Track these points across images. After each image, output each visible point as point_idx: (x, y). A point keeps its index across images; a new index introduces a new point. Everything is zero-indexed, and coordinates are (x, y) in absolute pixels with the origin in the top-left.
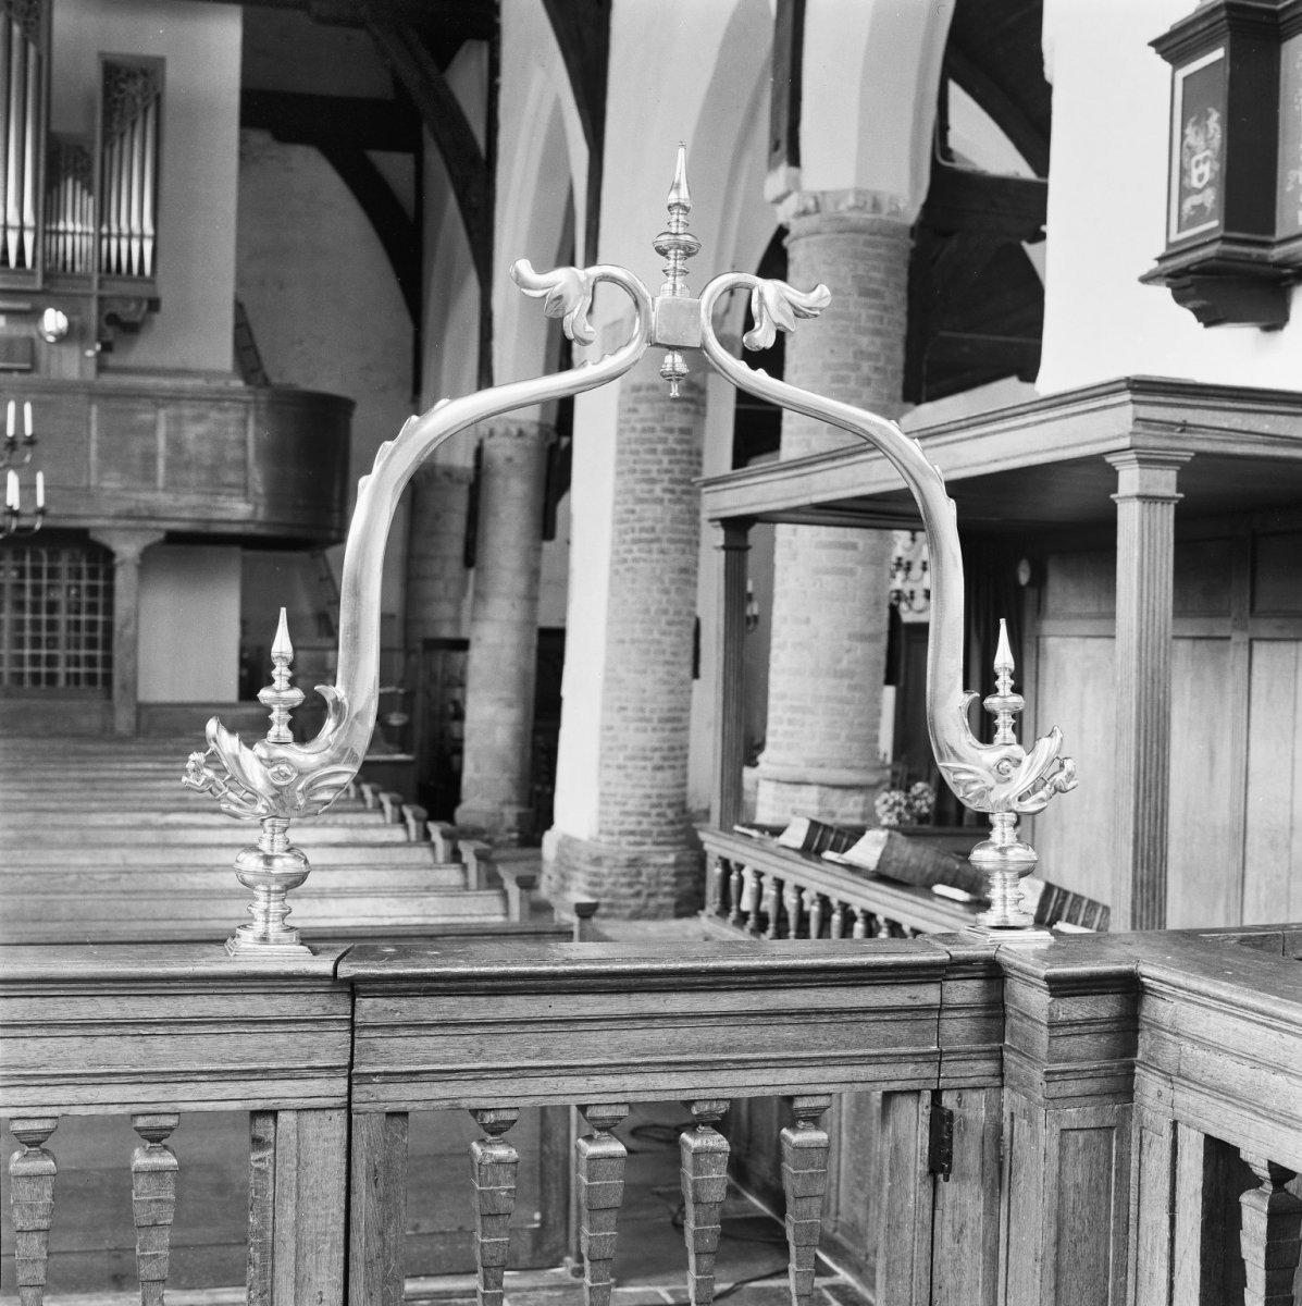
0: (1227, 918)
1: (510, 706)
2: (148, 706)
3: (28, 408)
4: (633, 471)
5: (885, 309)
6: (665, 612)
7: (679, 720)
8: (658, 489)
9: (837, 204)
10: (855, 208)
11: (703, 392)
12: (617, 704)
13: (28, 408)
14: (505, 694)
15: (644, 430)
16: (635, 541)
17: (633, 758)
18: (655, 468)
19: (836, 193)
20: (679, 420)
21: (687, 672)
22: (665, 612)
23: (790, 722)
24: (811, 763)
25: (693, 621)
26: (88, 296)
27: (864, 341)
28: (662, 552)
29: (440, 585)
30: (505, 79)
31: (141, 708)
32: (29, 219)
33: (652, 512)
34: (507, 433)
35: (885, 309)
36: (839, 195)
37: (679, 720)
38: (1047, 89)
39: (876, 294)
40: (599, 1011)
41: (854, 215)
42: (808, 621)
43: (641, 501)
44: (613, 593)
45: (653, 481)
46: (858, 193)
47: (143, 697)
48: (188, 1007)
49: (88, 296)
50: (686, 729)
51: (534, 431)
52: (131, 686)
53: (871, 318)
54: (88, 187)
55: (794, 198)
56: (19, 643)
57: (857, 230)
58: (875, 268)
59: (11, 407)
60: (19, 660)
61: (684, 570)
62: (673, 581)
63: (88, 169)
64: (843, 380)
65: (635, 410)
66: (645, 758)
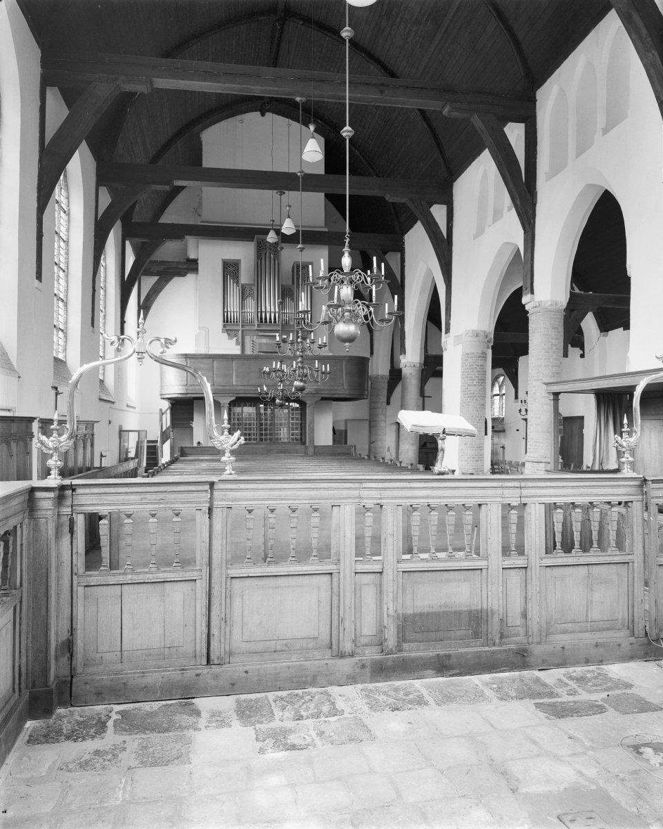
1: (413, 445)
2: (317, 447)
4: (467, 377)
5: (559, 332)
8: (475, 382)
9: (545, 304)
11: (486, 354)
14: (411, 441)
18: (473, 376)
20: (480, 363)
27: (554, 341)
28: (476, 400)
29: (381, 410)
30: (407, 264)
31: (315, 447)
32: (277, 310)
33: (473, 388)
35: (559, 332)
38: (627, 280)
39: (555, 328)
41: (549, 307)
42: (540, 418)
46: (551, 301)
47: (316, 444)
48: (620, 483)
51: (418, 365)
52: (312, 441)
53: (555, 335)
54: (293, 299)
55: (532, 303)
56: (261, 430)
57: (551, 311)
59: (328, 370)
60: (261, 434)
63: (292, 295)
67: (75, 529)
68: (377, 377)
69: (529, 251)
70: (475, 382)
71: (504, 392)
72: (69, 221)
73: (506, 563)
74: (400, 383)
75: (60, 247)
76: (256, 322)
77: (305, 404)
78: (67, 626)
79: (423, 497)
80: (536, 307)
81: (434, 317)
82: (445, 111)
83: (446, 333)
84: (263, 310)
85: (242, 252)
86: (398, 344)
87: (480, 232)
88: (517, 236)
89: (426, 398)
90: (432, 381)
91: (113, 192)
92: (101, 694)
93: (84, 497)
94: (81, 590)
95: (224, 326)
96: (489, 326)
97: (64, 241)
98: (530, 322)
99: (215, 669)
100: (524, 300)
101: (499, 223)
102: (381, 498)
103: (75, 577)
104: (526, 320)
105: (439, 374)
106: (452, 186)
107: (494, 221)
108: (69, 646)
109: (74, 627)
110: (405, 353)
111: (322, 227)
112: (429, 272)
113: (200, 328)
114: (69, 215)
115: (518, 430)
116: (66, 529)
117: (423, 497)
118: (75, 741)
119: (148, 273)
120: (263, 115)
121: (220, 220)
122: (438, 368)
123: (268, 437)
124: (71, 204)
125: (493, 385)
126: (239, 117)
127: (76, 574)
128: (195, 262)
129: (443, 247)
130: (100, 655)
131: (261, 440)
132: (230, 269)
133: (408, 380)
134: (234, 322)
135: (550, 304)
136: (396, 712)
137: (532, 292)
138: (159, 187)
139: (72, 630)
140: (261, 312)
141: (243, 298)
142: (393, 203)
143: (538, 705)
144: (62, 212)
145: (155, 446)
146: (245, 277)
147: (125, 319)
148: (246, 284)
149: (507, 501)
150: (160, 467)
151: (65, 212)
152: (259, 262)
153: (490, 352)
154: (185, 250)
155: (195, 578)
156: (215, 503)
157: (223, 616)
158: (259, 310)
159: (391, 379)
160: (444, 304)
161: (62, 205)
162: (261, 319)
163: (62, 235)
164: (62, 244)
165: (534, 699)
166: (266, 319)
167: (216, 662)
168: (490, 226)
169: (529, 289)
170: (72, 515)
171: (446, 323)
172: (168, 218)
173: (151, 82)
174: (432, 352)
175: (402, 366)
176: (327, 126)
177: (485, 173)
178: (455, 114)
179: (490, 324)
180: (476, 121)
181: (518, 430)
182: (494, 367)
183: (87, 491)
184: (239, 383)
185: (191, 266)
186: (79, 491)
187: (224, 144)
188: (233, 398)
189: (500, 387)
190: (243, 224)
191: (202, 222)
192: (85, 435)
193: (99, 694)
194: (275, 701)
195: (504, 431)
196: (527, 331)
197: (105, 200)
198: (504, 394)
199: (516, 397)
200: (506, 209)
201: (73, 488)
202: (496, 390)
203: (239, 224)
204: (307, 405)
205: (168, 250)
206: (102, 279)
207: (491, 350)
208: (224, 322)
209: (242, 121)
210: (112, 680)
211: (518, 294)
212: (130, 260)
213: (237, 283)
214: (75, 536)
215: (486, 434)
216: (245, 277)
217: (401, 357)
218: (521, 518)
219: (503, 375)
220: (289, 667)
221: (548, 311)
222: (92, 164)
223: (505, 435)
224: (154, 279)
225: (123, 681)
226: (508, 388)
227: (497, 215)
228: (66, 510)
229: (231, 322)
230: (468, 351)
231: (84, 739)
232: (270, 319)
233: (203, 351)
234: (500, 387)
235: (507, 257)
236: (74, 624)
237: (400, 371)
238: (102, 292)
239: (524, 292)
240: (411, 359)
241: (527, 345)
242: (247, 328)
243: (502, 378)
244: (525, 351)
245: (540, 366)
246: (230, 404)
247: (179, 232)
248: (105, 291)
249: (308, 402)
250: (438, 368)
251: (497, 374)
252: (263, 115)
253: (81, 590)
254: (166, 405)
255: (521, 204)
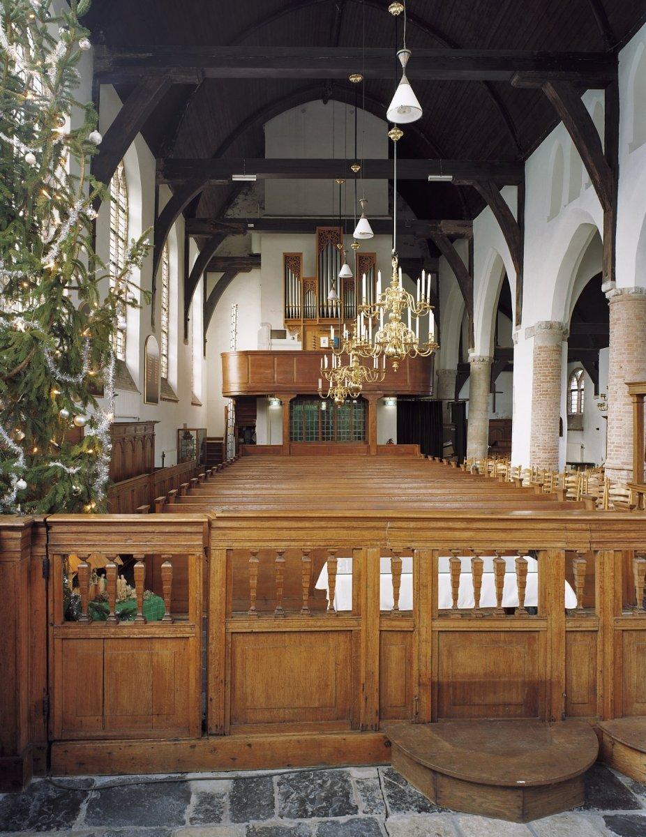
0: (270, 438)
2: (380, 446)
3: (429, 276)
6: (552, 416)
7: (556, 449)
8: (548, 378)
10: (635, 293)
12: (536, 445)
13: (429, 276)
15: (543, 360)
16: (541, 395)
17: (542, 461)
19: (628, 289)
21: (558, 434)
22: (552, 416)
23: (616, 451)
24: (623, 463)
25: (559, 418)
26: (300, 326)
33: (545, 386)
34: (479, 361)
36: (629, 289)
37: (556, 449)
40: (493, 527)
43: (543, 382)
44: (533, 410)
45: (547, 376)
49: (300, 326)
50: (558, 452)
51: (487, 359)
55: (613, 290)
58: (641, 311)
61: (557, 403)
62: (553, 407)
64: (631, 345)
65: (540, 354)
66: (546, 461)
67: (51, 573)
68: (445, 371)
69: (610, 231)
70: (548, 378)
71: (582, 387)
72: (128, 220)
73: (569, 625)
74: (469, 378)
75: (118, 246)
76: (318, 316)
77: (367, 401)
78: (43, 684)
79: (464, 541)
80: (617, 295)
81: (504, 307)
82: (514, 82)
83: (517, 325)
84: (325, 304)
85: (304, 245)
86: (465, 340)
87: (554, 213)
88: (597, 217)
89: (496, 394)
90: (503, 376)
91: (174, 188)
92: (84, 764)
93: (62, 536)
94: (58, 642)
95: (286, 322)
96: (563, 316)
97: (123, 241)
98: (611, 312)
99: (213, 741)
100: (604, 288)
101: (575, 203)
102: (412, 541)
103: (51, 628)
104: (607, 310)
105: (510, 368)
106: (524, 165)
107: (570, 200)
108: (46, 708)
109: (50, 685)
110: (473, 346)
111: (386, 216)
112: (499, 258)
113: (263, 324)
114: (127, 214)
115: (598, 429)
116: (40, 573)
117: (464, 541)
118: (39, 829)
119: (213, 268)
120: (325, 103)
121: (282, 213)
122: (510, 362)
123: (325, 436)
124: (130, 203)
125: (570, 380)
126: (300, 107)
127: (52, 625)
128: (258, 256)
129: (515, 233)
130: (80, 718)
131: (323, 439)
132: (292, 262)
133: (477, 375)
134: (295, 317)
135: (634, 291)
136: (423, 813)
137: (613, 279)
138: (219, 182)
139: (48, 690)
140: (292, 307)
141: (305, 293)
142: (459, 186)
143: (610, 822)
144: (120, 212)
145: (221, 444)
146: (307, 270)
147: (189, 317)
148: (308, 278)
149: (571, 547)
150: (228, 462)
151: (124, 211)
152: (321, 255)
153: (566, 345)
154: (249, 246)
155: (188, 635)
156: (212, 544)
157: (222, 677)
158: (321, 304)
159: (459, 374)
160: (515, 292)
161: (121, 204)
162: (323, 313)
163: (120, 234)
164: (121, 243)
165: (604, 808)
166: (328, 313)
167: (214, 731)
168: (565, 206)
169: (610, 275)
170: (47, 556)
171: (517, 314)
172: (232, 213)
173: (203, 73)
174: (503, 345)
175: (470, 360)
176: (370, 99)
177: (560, 149)
178: (527, 84)
179: (565, 315)
180: (550, 91)
181: (598, 429)
182: (570, 361)
183: (65, 529)
184: (300, 381)
185: (253, 261)
186: (55, 529)
187: (287, 135)
188: (295, 396)
189: (579, 382)
190: (305, 216)
191: (265, 216)
192: (144, 437)
193: (81, 764)
194: (279, 784)
195: (583, 430)
196: (608, 321)
197: (167, 195)
198: (583, 390)
199: (596, 393)
200: (584, 186)
201: (48, 526)
202: (574, 385)
203: (302, 216)
204: (370, 403)
205: (231, 245)
206: (164, 277)
207: (567, 343)
208: (286, 317)
209: (304, 111)
210: (95, 749)
211: (597, 281)
212: (194, 255)
213: (299, 277)
214: (50, 582)
215: (561, 435)
216: (307, 270)
217: (470, 350)
218: (590, 566)
219: (581, 369)
220: (299, 742)
221: (630, 299)
222: (151, 161)
223: (583, 435)
224: (220, 275)
225: (109, 751)
226: (587, 383)
227: (574, 195)
228: (41, 551)
229: (292, 317)
230: (540, 345)
231: (49, 828)
232: (332, 313)
233: (265, 348)
234: (578, 382)
235: (586, 237)
236: (51, 682)
237: (468, 365)
238: (165, 290)
239: (604, 278)
240: (480, 351)
241: (608, 336)
242: (308, 323)
243: (580, 372)
244: (606, 343)
245: (623, 362)
246: (291, 401)
247: (240, 227)
248: (168, 289)
249: (370, 398)
250: (510, 362)
251: (575, 367)
252: (325, 103)
253: (58, 642)
254: (230, 403)
255: (601, 181)
